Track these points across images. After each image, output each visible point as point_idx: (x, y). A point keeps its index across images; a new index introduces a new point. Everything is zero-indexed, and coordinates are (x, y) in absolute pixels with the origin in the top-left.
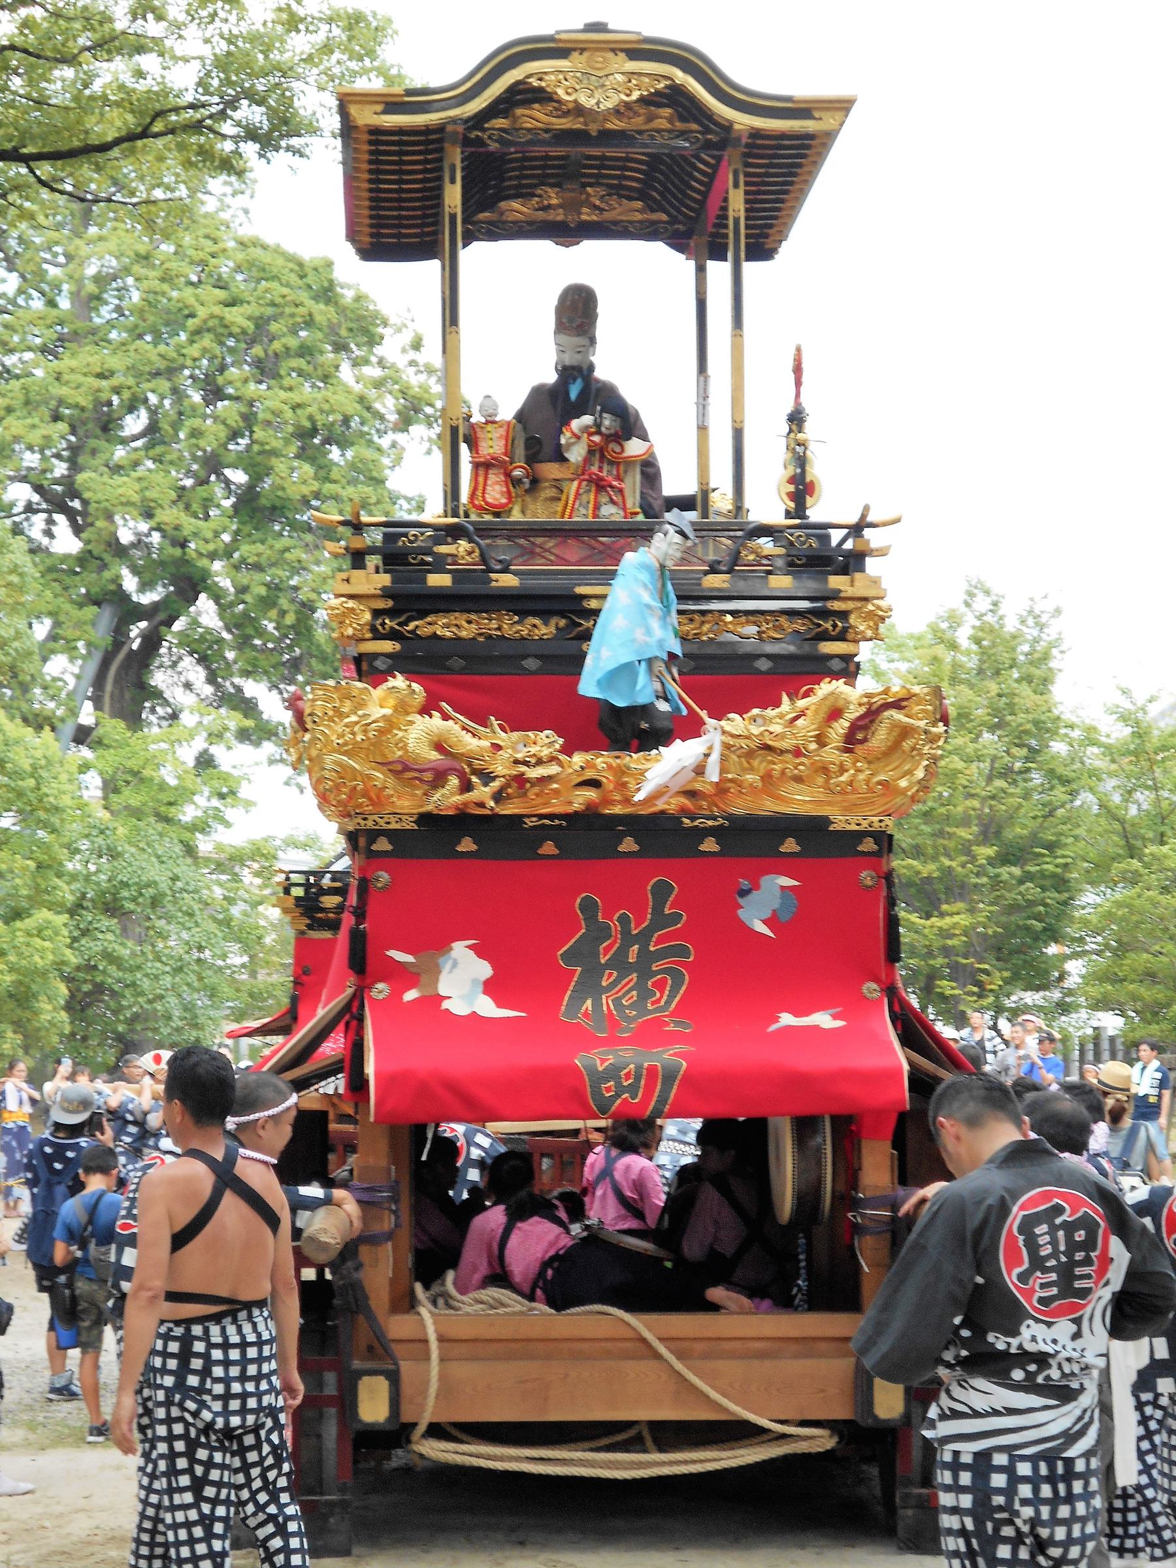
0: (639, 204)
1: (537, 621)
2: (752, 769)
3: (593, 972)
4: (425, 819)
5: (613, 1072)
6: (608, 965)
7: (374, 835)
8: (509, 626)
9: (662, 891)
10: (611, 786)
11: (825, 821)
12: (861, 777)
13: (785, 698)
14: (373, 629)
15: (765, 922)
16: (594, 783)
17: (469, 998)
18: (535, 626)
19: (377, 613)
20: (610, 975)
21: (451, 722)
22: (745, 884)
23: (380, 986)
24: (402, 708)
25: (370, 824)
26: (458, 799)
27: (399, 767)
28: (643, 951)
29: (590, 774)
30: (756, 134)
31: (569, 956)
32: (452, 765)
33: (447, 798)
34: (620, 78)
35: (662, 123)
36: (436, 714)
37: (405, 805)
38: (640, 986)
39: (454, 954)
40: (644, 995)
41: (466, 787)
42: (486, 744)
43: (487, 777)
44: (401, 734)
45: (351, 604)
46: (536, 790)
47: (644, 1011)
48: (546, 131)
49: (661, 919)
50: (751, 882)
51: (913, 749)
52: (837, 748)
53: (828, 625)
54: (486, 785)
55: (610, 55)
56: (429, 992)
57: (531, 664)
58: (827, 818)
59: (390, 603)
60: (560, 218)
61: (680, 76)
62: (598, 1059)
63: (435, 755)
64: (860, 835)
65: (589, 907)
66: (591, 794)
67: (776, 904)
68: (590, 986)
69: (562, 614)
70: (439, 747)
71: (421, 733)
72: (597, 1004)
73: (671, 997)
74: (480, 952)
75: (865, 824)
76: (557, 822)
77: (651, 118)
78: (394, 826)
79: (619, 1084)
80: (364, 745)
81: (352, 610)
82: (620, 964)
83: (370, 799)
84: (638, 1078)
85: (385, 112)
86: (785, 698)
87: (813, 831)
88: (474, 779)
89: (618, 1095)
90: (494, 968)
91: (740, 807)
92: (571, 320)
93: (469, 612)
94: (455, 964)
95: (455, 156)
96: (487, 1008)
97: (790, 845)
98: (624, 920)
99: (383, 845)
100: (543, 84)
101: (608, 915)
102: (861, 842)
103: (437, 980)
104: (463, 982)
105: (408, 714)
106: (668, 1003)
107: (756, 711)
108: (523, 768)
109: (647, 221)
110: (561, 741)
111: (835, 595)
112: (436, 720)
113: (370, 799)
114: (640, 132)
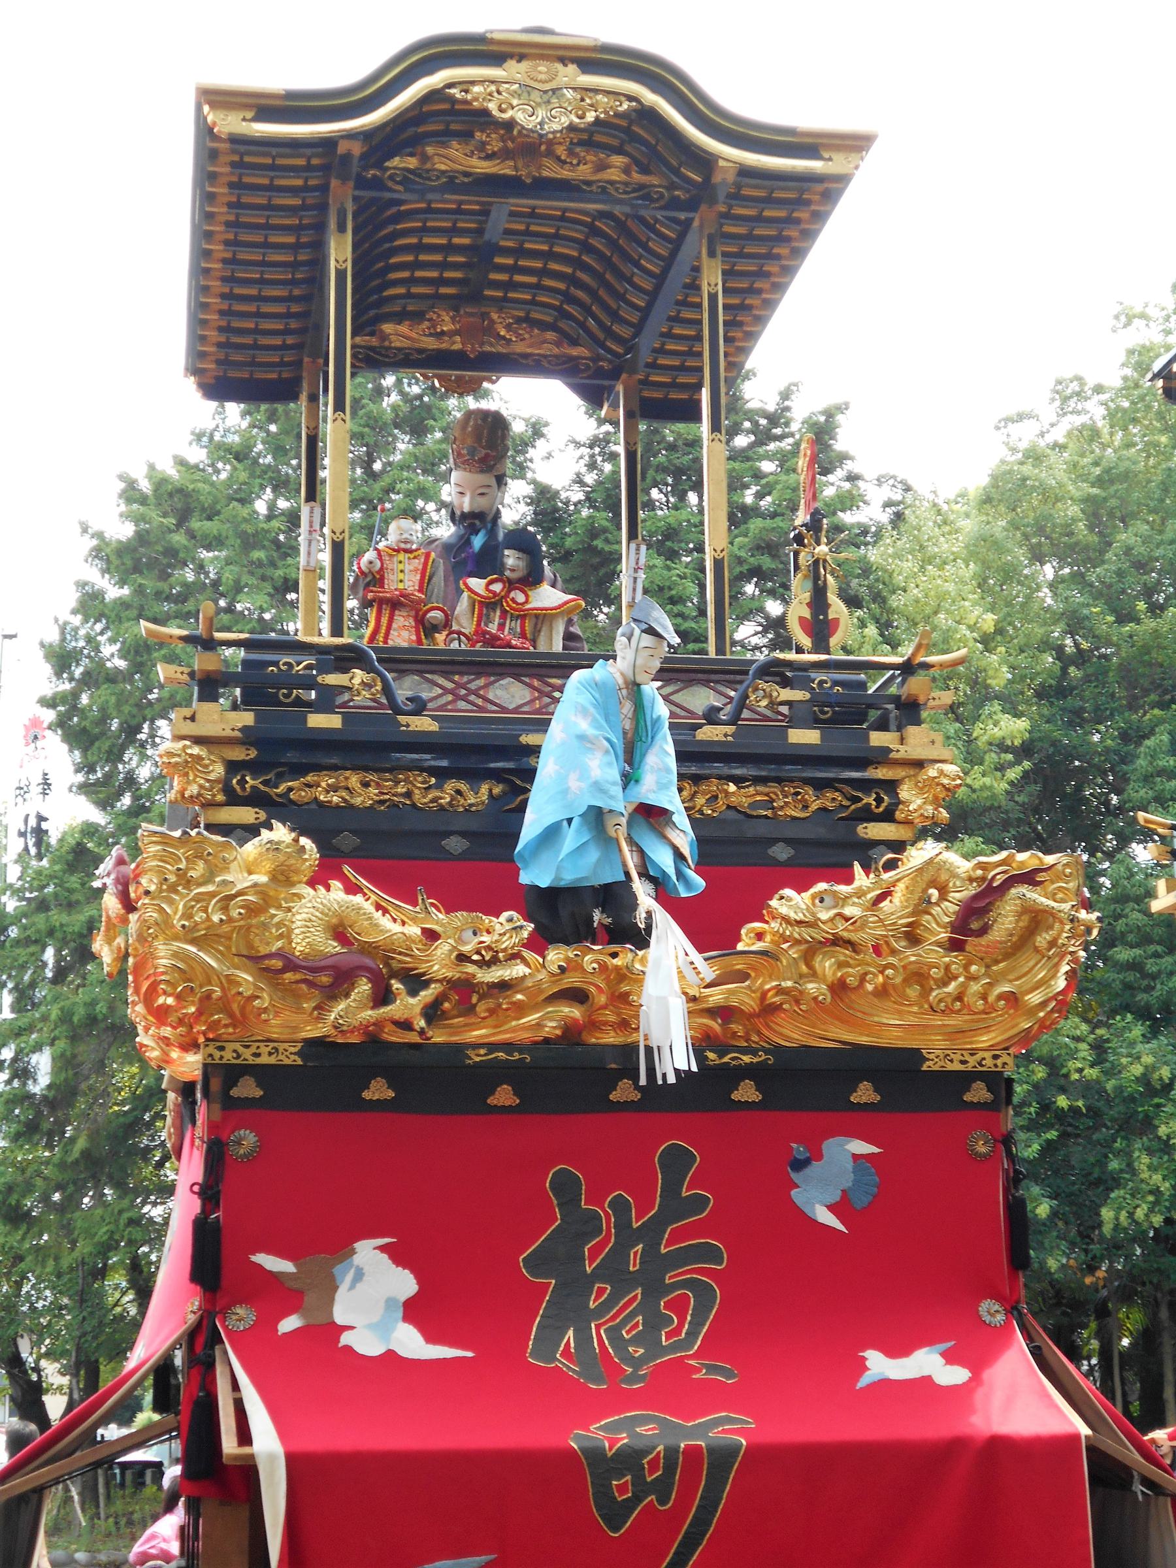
0: (550, 335)
1: (463, 786)
2: (814, 975)
3: (575, 1287)
4: (314, 1046)
5: (629, 1459)
6: (596, 1276)
7: (233, 1073)
8: (423, 792)
9: (676, 1162)
10: (603, 999)
11: (915, 1056)
12: (975, 987)
13: (857, 868)
14: (228, 790)
15: (831, 1208)
16: (577, 996)
17: (382, 1328)
18: (459, 792)
19: (233, 767)
20: (601, 1291)
21: (358, 899)
22: (799, 1150)
23: (241, 1311)
24: (282, 877)
25: (228, 1056)
26: (369, 1014)
27: (278, 964)
28: (651, 1252)
29: (572, 980)
30: (746, 172)
31: (537, 1263)
32: (358, 964)
33: (352, 1011)
34: (569, 94)
35: (614, 174)
36: (336, 884)
37: (288, 1028)
38: (648, 1308)
39: (357, 1259)
40: (655, 1323)
41: (382, 997)
42: (414, 930)
43: (416, 982)
44: (280, 915)
45: (195, 750)
46: (490, 1003)
47: (655, 1348)
48: (466, 174)
49: (675, 1207)
50: (808, 1148)
51: (1053, 943)
52: (939, 944)
53: (870, 800)
54: (413, 993)
55: (559, 66)
56: (321, 1320)
57: (455, 844)
58: (918, 1051)
59: (253, 754)
60: (457, 346)
61: (650, 97)
62: (603, 1433)
63: (334, 947)
64: (965, 1079)
65: (566, 1187)
66: (573, 1012)
67: (847, 1181)
68: (570, 1309)
69: (497, 776)
70: (340, 934)
71: (313, 913)
72: (583, 1338)
73: (696, 1325)
74: (398, 1255)
75: (972, 1061)
76: (517, 1056)
77: (602, 167)
78: (265, 1060)
79: (639, 1479)
80: (226, 928)
81: (199, 758)
82: (614, 1271)
83: (231, 1015)
84: (670, 1468)
85: (256, 119)
86: (857, 868)
87: (897, 1070)
88: (396, 985)
89: (637, 1499)
90: (420, 1281)
91: (791, 1033)
92: (472, 452)
93: (366, 769)
94: (359, 1275)
95: (343, 195)
96: (411, 1343)
97: (865, 1093)
98: (620, 1206)
99: (248, 1089)
100: (469, 97)
101: (596, 1197)
102: (968, 1089)
103: (331, 1301)
104: (371, 1302)
105: (293, 884)
106: (693, 1334)
107: (822, 886)
108: (471, 969)
109: (565, 355)
110: (531, 927)
111: (882, 756)
112: (336, 893)
113: (231, 1015)
114: (588, 183)
